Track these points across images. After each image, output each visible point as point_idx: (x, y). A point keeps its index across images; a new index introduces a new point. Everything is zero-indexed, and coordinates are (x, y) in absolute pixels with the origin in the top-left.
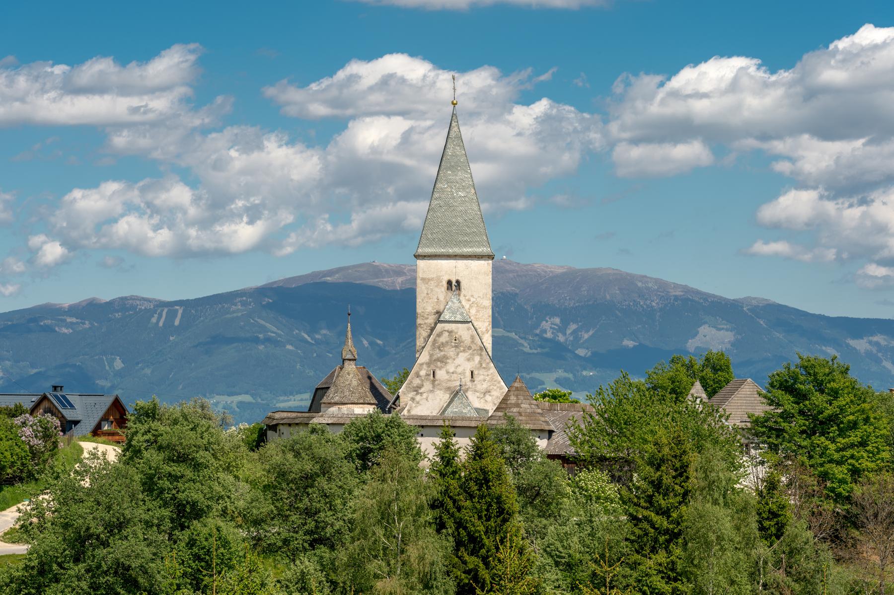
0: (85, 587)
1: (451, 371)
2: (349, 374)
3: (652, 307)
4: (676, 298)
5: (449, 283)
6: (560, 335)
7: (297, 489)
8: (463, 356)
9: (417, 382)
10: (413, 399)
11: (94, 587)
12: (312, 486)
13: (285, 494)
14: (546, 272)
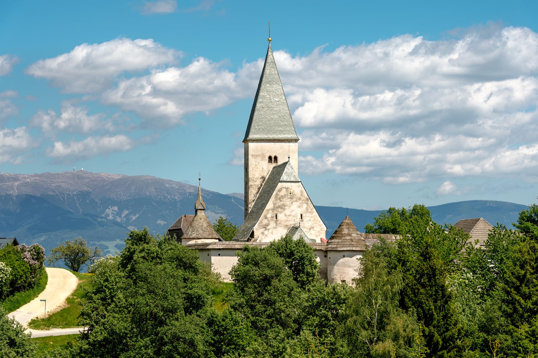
0: (151, 354)
1: (288, 214)
2: (201, 219)
3: (175, 199)
4: (190, 194)
5: (270, 158)
6: (118, 217)
7: (259, 286)
8: (296, 204)
9: (265, 222)
10: (263, 233)
11: (158, 353)
12: (269, 284)
13: (251, 291)
14: (108, 178)
